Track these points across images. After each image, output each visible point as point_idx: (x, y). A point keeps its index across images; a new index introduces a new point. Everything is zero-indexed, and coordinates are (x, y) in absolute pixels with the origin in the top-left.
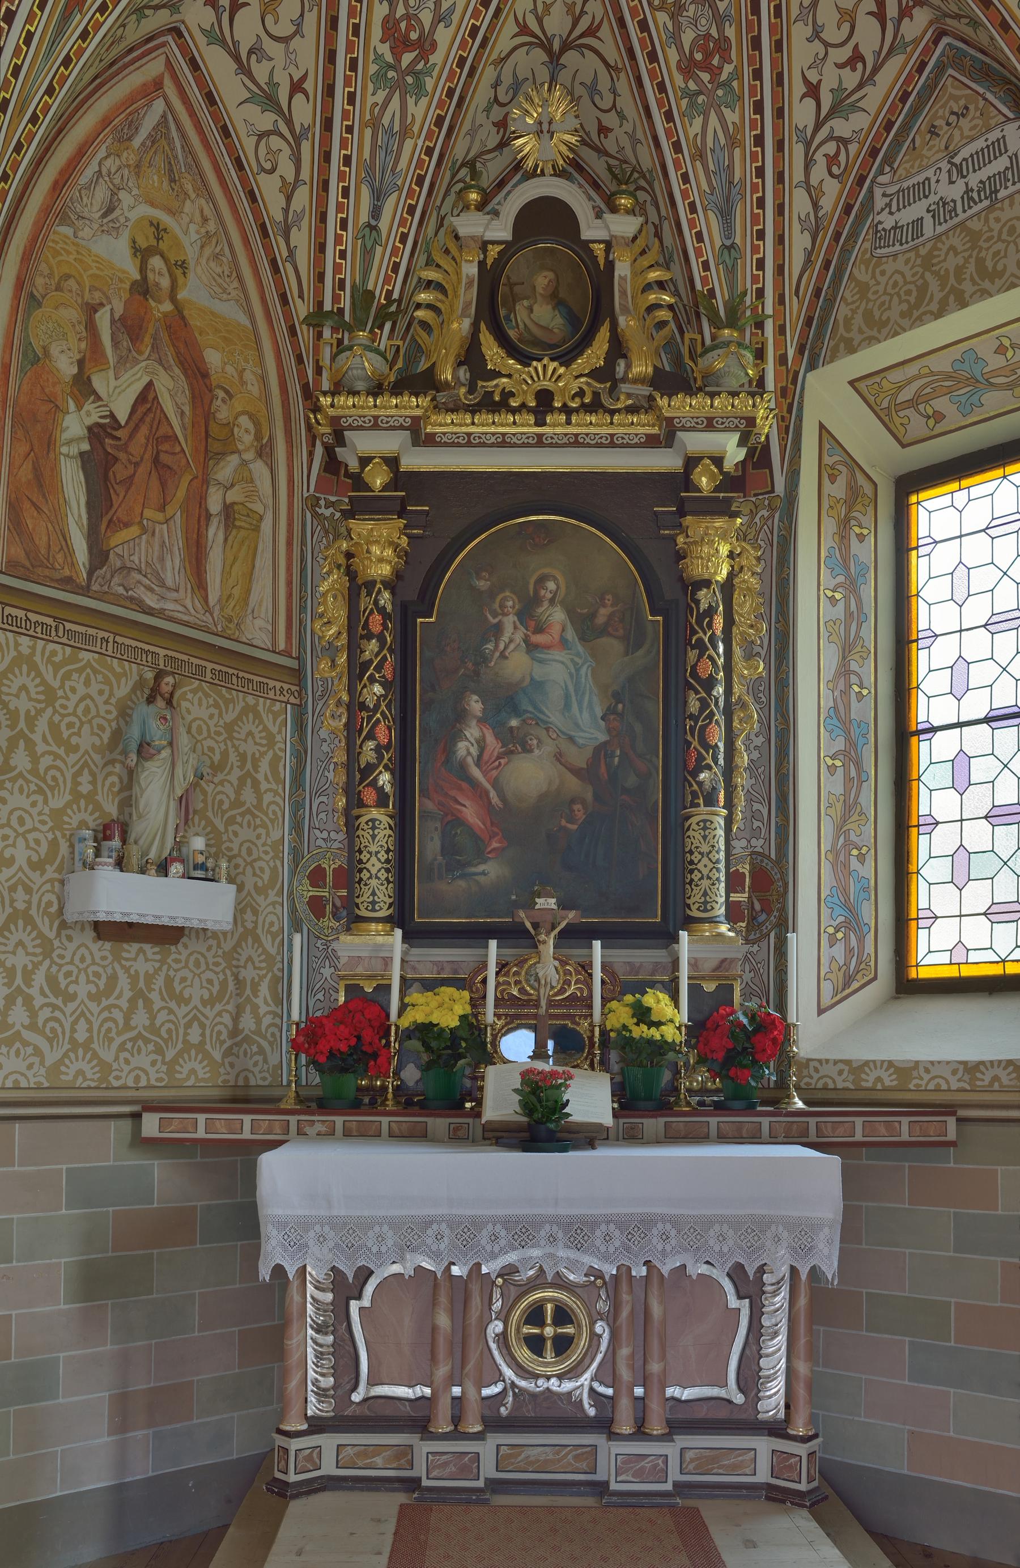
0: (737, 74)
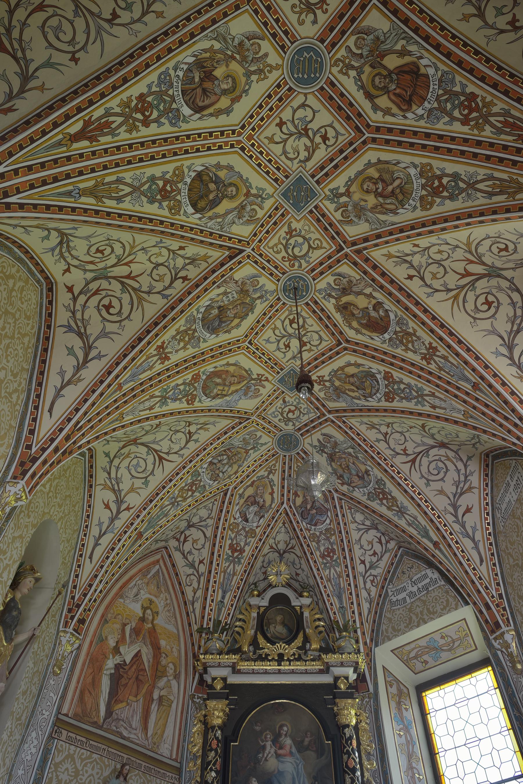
0: (339, 558)
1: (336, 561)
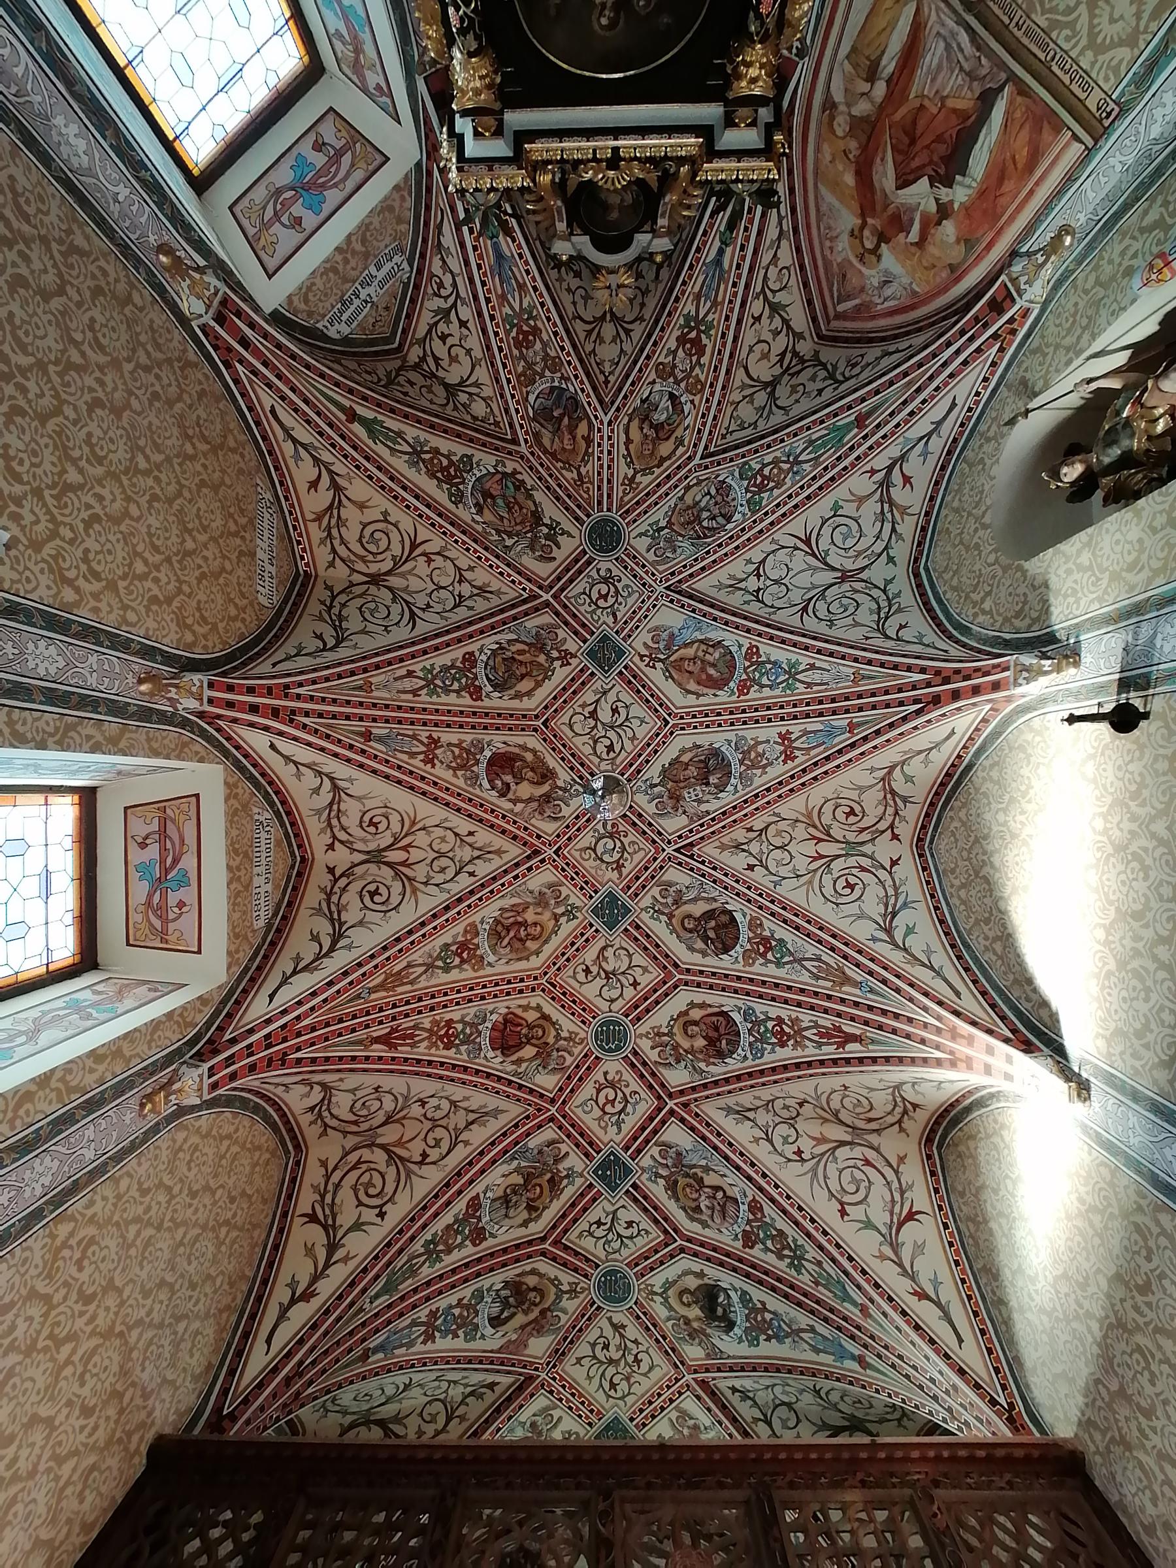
1: (513, 326)
